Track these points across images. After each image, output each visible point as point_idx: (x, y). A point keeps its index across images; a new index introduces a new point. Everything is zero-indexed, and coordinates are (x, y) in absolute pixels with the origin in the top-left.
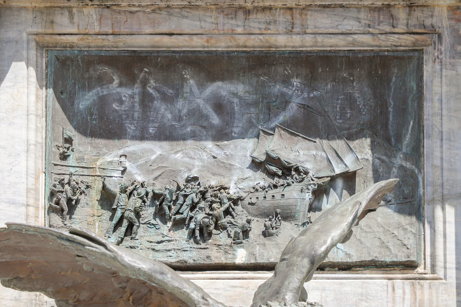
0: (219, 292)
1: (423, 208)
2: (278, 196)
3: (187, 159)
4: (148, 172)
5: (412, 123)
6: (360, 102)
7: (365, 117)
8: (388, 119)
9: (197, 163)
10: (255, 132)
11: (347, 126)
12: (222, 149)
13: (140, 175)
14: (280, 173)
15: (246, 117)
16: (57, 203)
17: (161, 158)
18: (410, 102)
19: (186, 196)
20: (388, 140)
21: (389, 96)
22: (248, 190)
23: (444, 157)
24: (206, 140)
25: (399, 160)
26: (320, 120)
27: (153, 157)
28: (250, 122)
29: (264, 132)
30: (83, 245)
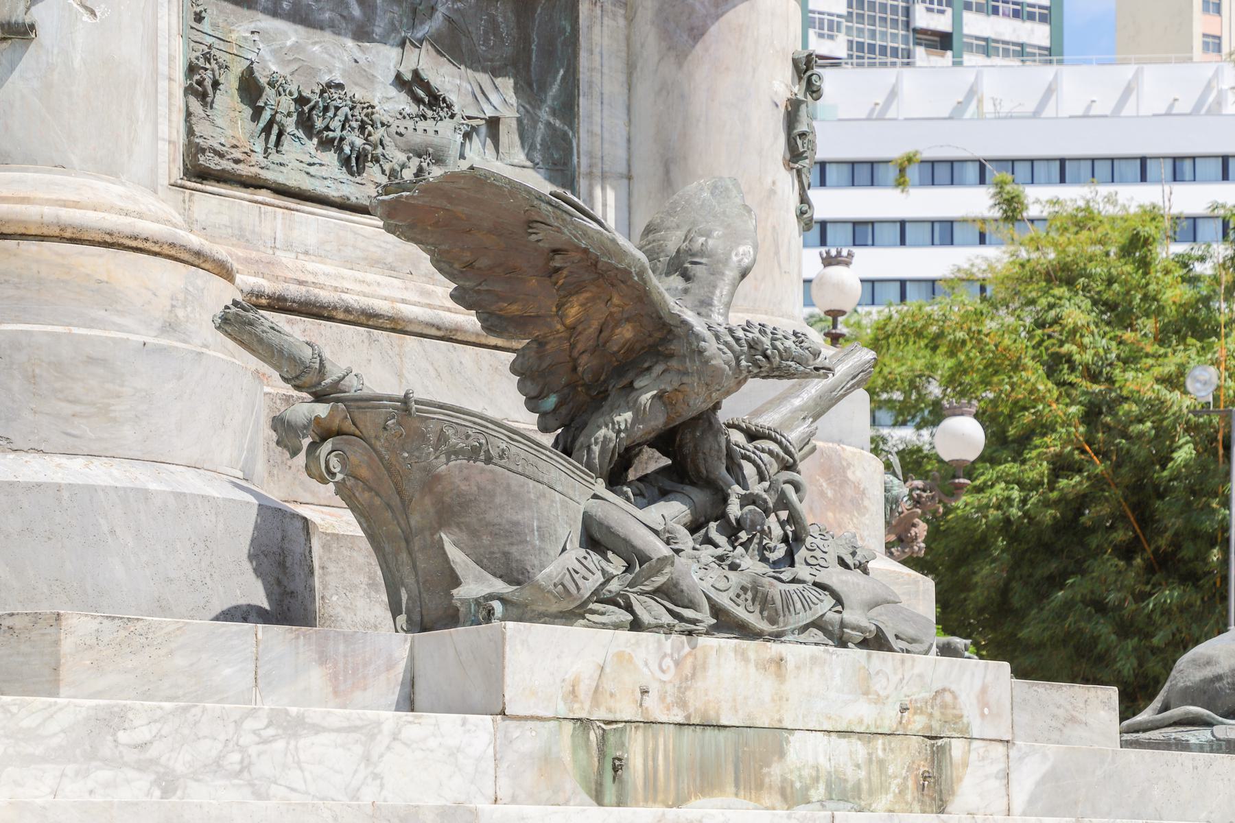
0: (389, 246)
1: (578, 182)
2: (431, 132)
3: (326, 56)
4: (284, 62)
5: (562, 72)
6: (504, 30)
7: (508, 51)
8: (530, 58)
9: (338, 64)
10: (398, 39)
11: (490, 56)
12: (364, 53)
13: (273, 64)
14: (426, 100)
15: (389, 15)
16: (200, 83)
17: (297, 47)
18: (559, 46)
19: (337, 108)
20: (530, 85)
21: (533, 30)
22: (393, 114)
23: (605, 125)
24: (345, 35)
25: (544, 114)
26: (464, 41)
27: (289, 43)
28: (392, 24)
29: (410, 41)
30: (572, 216)
